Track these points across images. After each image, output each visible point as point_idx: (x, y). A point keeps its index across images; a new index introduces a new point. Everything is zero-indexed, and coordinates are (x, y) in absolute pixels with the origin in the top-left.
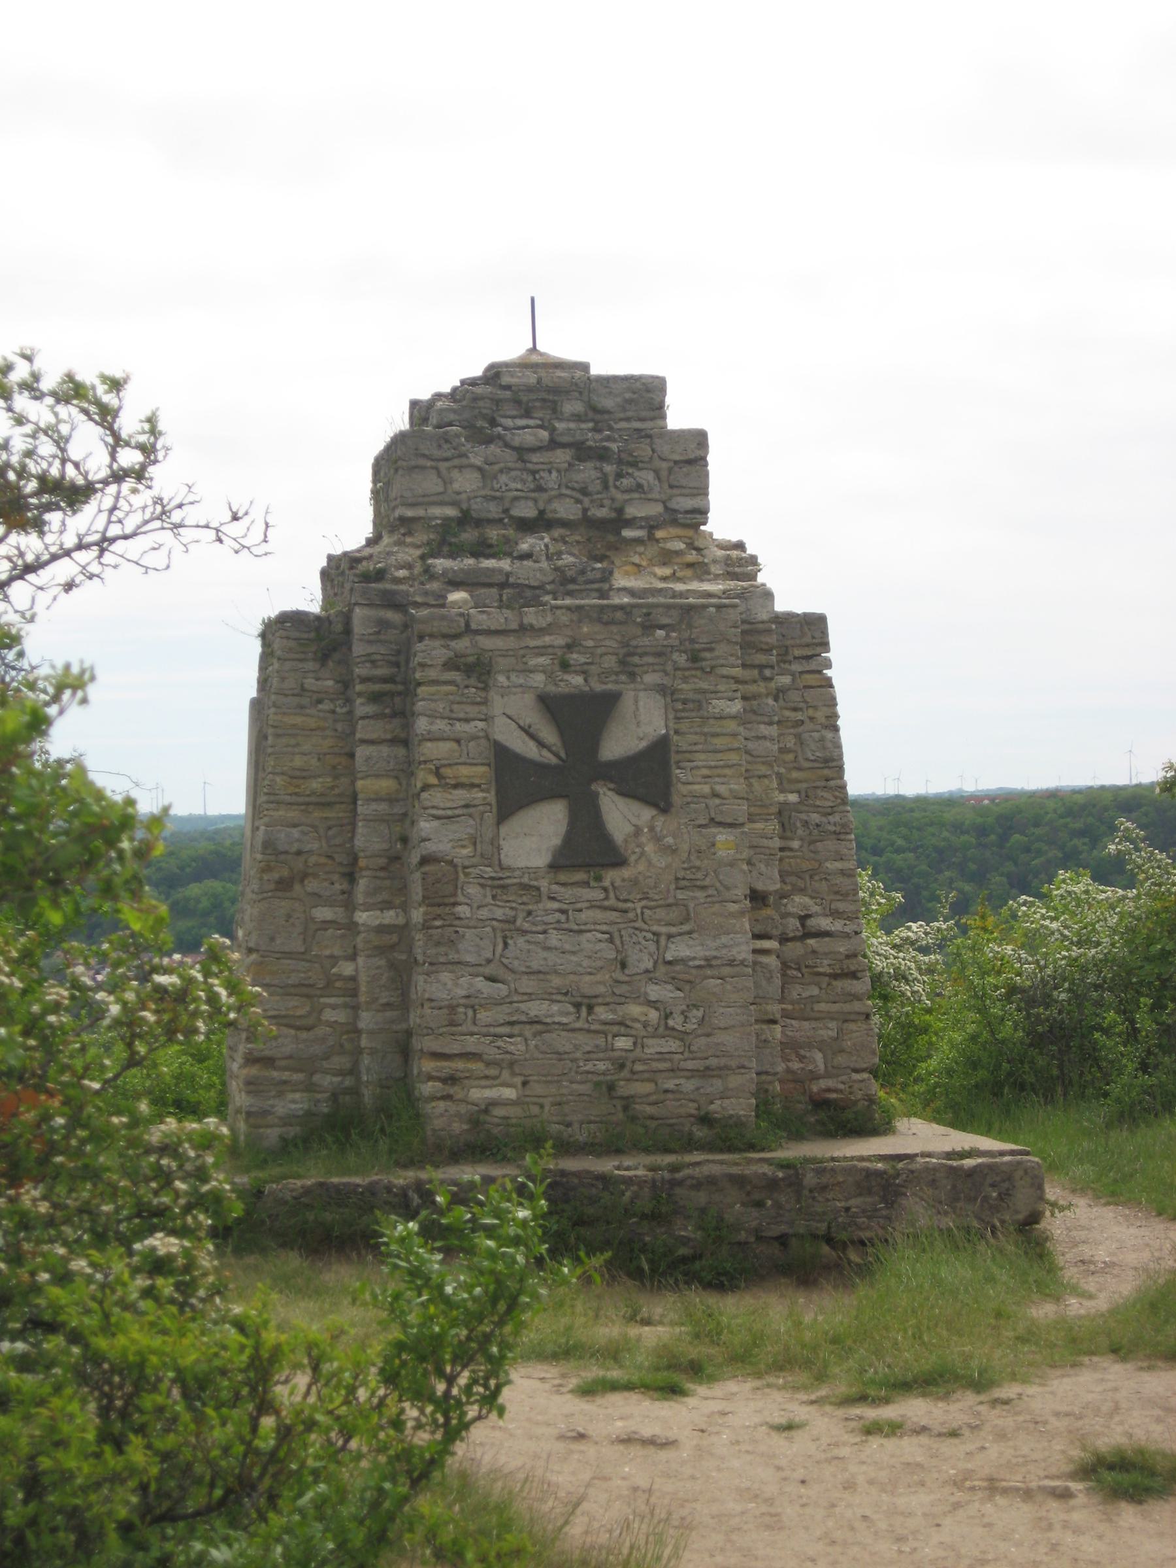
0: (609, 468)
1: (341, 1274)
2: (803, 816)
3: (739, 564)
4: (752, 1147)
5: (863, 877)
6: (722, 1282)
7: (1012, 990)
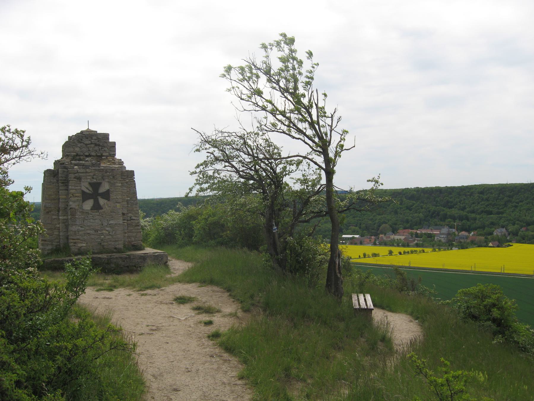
0: (100, 147)
1: (58, 274)
3: (121, 162)
4: (123, 252)
5: (140, 211)
6: (118, 273)
7: (163, 228)
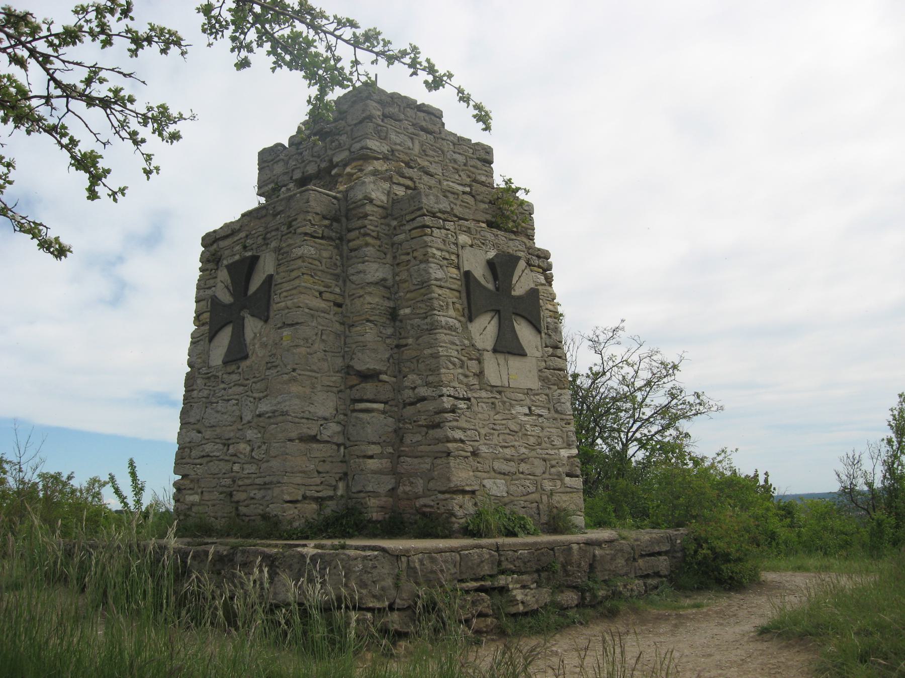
2: (411, 322)
